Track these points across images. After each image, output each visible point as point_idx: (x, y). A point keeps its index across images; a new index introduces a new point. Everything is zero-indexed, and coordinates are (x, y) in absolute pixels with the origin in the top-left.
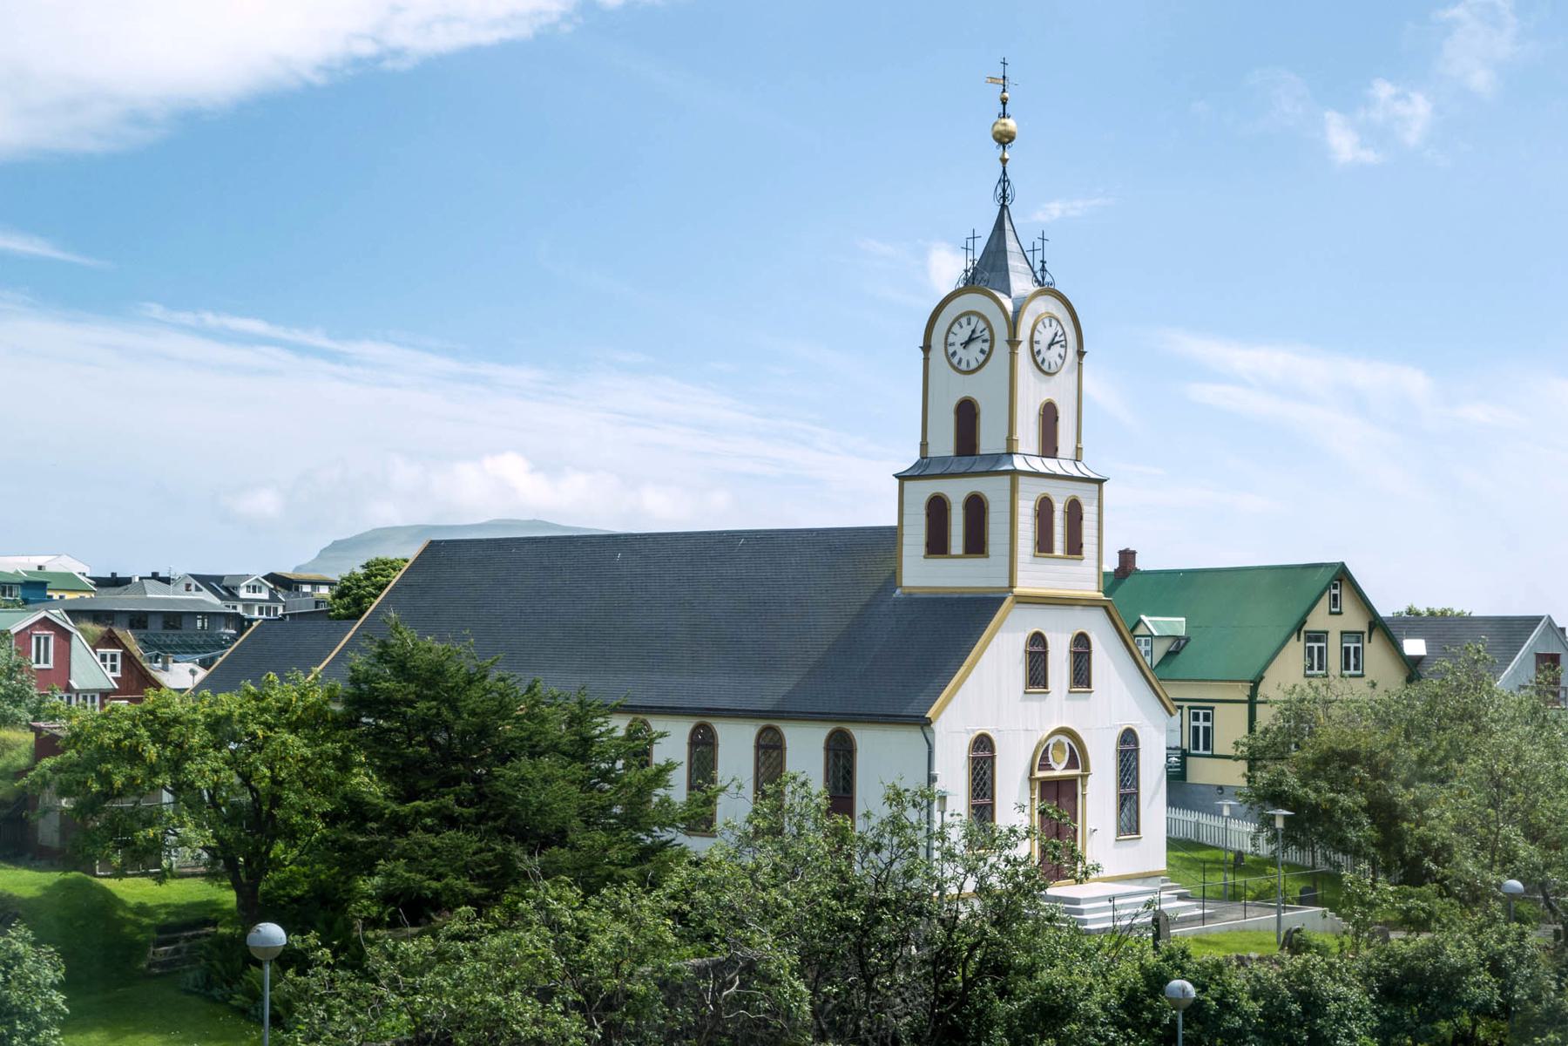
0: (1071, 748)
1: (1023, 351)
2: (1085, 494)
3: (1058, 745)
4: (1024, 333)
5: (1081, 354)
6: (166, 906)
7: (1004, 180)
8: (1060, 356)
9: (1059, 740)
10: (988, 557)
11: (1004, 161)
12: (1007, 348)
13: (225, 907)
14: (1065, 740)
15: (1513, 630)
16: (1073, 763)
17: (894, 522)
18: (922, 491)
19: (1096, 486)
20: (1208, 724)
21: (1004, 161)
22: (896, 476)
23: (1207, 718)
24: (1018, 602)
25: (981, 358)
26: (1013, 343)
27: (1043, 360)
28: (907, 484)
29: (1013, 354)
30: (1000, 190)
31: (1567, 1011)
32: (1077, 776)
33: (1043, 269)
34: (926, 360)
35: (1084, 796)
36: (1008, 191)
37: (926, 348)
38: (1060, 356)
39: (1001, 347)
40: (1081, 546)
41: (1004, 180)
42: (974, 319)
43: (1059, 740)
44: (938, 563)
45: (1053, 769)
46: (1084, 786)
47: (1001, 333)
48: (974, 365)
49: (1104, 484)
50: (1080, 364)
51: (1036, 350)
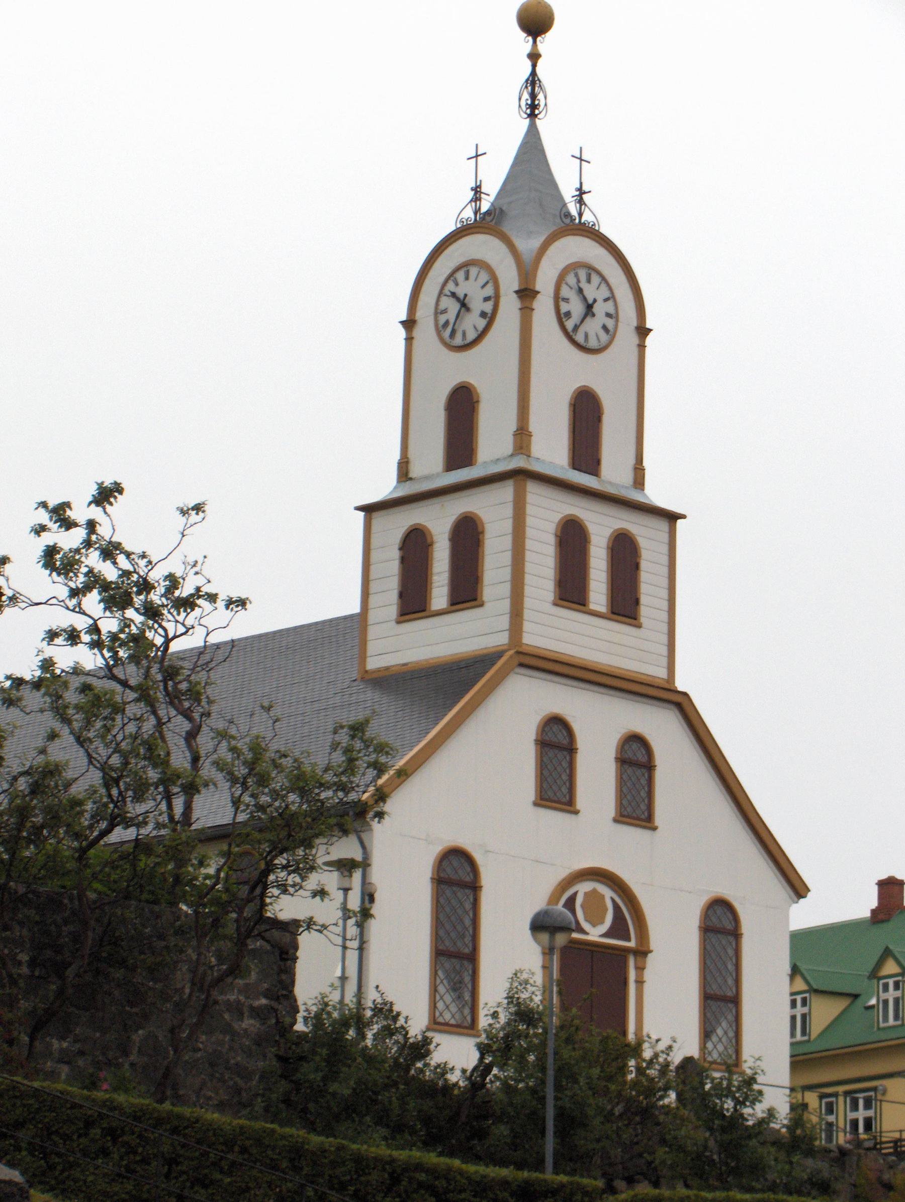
0: (616, 907)
1: (543, 306)
2: (642, 529)
3: (594, 901)
4: (545, 281)
5: (643, 332)
6: (545, 1144)
7: (533, 81)
8: (605, 328)
9: (594, 891)
10: (482, 605)
11: (534, 57)
12: (635, 340)
13: (783, 1141)
14: (607, 893)
15: (814, 1198)
16: (619, 929)
17: (354, 607)
19: (664, 525)
20: (870, 1113)
21: (534, 57)
22: (359, 509)
23: (868, 1105)
24: (521, 665)
25: (482, 323)
26: (527, 294)
27: (586, 336)
28: (379, 520)
29: (526, 311)
30: (526, 96)
31: (904, 1149)
32: (627, 950)
33: (581, 202)
34: (409, 340)
35: (640, 982)
36: (541, 96)
37: (409, 324)
38: (605, 328)
39: (510, 305)
40: (637, 602)
41: (533, 81)
42: (473, 271)
43: (594, 891)
44: (419, 628)
45: (586, 933)
46: (640, 969)
47: (510, 281)
48: (471, 336)
49: (680, 522)
50: (642, 347)
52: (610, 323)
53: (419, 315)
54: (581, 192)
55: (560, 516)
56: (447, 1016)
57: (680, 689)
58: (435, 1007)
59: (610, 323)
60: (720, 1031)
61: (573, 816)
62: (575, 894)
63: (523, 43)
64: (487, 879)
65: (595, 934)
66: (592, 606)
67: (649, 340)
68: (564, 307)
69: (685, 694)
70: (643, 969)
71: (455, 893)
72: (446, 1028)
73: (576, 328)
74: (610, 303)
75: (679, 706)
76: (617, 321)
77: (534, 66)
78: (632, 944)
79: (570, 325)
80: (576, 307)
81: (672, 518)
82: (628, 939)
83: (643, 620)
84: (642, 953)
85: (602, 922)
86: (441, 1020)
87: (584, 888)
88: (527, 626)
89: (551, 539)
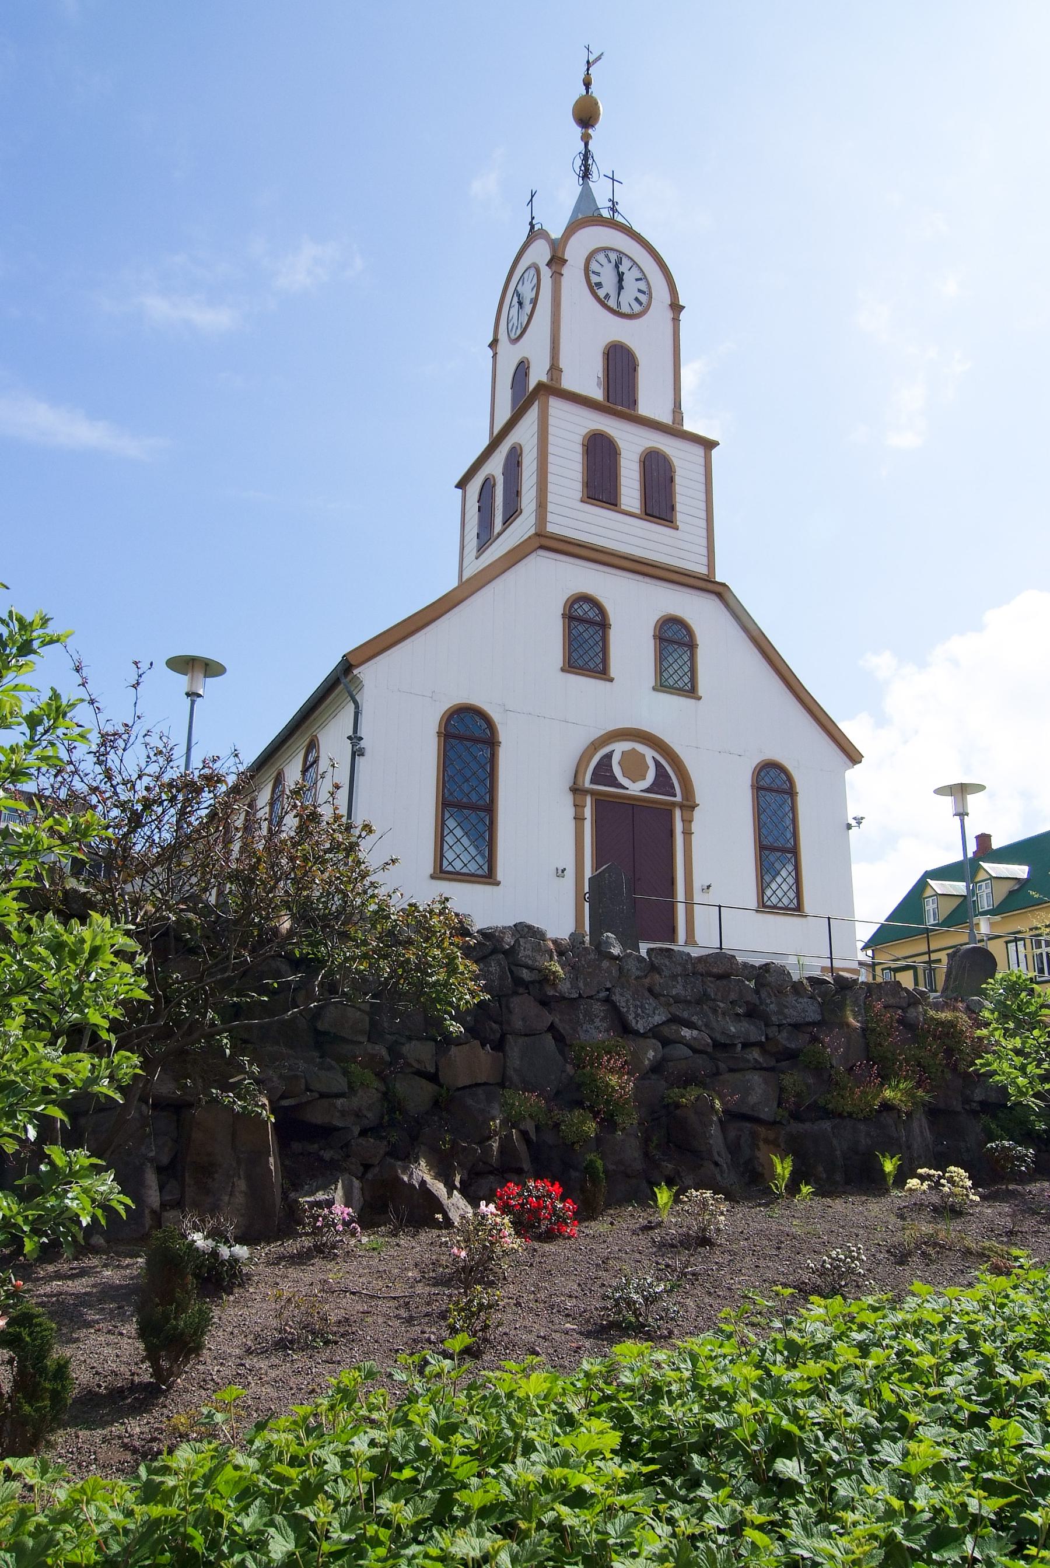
0: (658, 764)
5: (676, 308)
12: (670, 315)
14: (649, 754)
16: (662, 783)
18: (474, 487)
19: (699, 451)
24: (542, 547)
35: (688, 833)
40: (673, 508)
46: (687, 822)
50: (676, 320)
51: (602, 296)
52: (642, 285)
53: (499, 337)
54: (614, 203)
55: (584, 431)
56: (458, 865)
57: (718, 579)
58: (442, 856)
59: (643, 298)
60: (784, 873)
61: (608, 683)
62: (609, 756)
63: (578, 131)
64: (504, 735)
65: (635, 788)
66: (623, 507)
67: (683, 316)
68: (594, 279)
69: (724, 585)
70: (691, 821)
71: (468, 749)
72: (473, 879)
73: (619, 304)
74: (634, 269)
75: (719, 595)
76: (651, 297)
77: (586, 145)
78: (678, 798)
79: (612, 303)
80: (607, 278)
81: (709, 445)
82: (675, 796)
83: (678, 523)
84: (689, 806)
85: (643, 777)
86: (769, 903)
87: (620, 748)
88: (550, 517)
89: (579, 449)
